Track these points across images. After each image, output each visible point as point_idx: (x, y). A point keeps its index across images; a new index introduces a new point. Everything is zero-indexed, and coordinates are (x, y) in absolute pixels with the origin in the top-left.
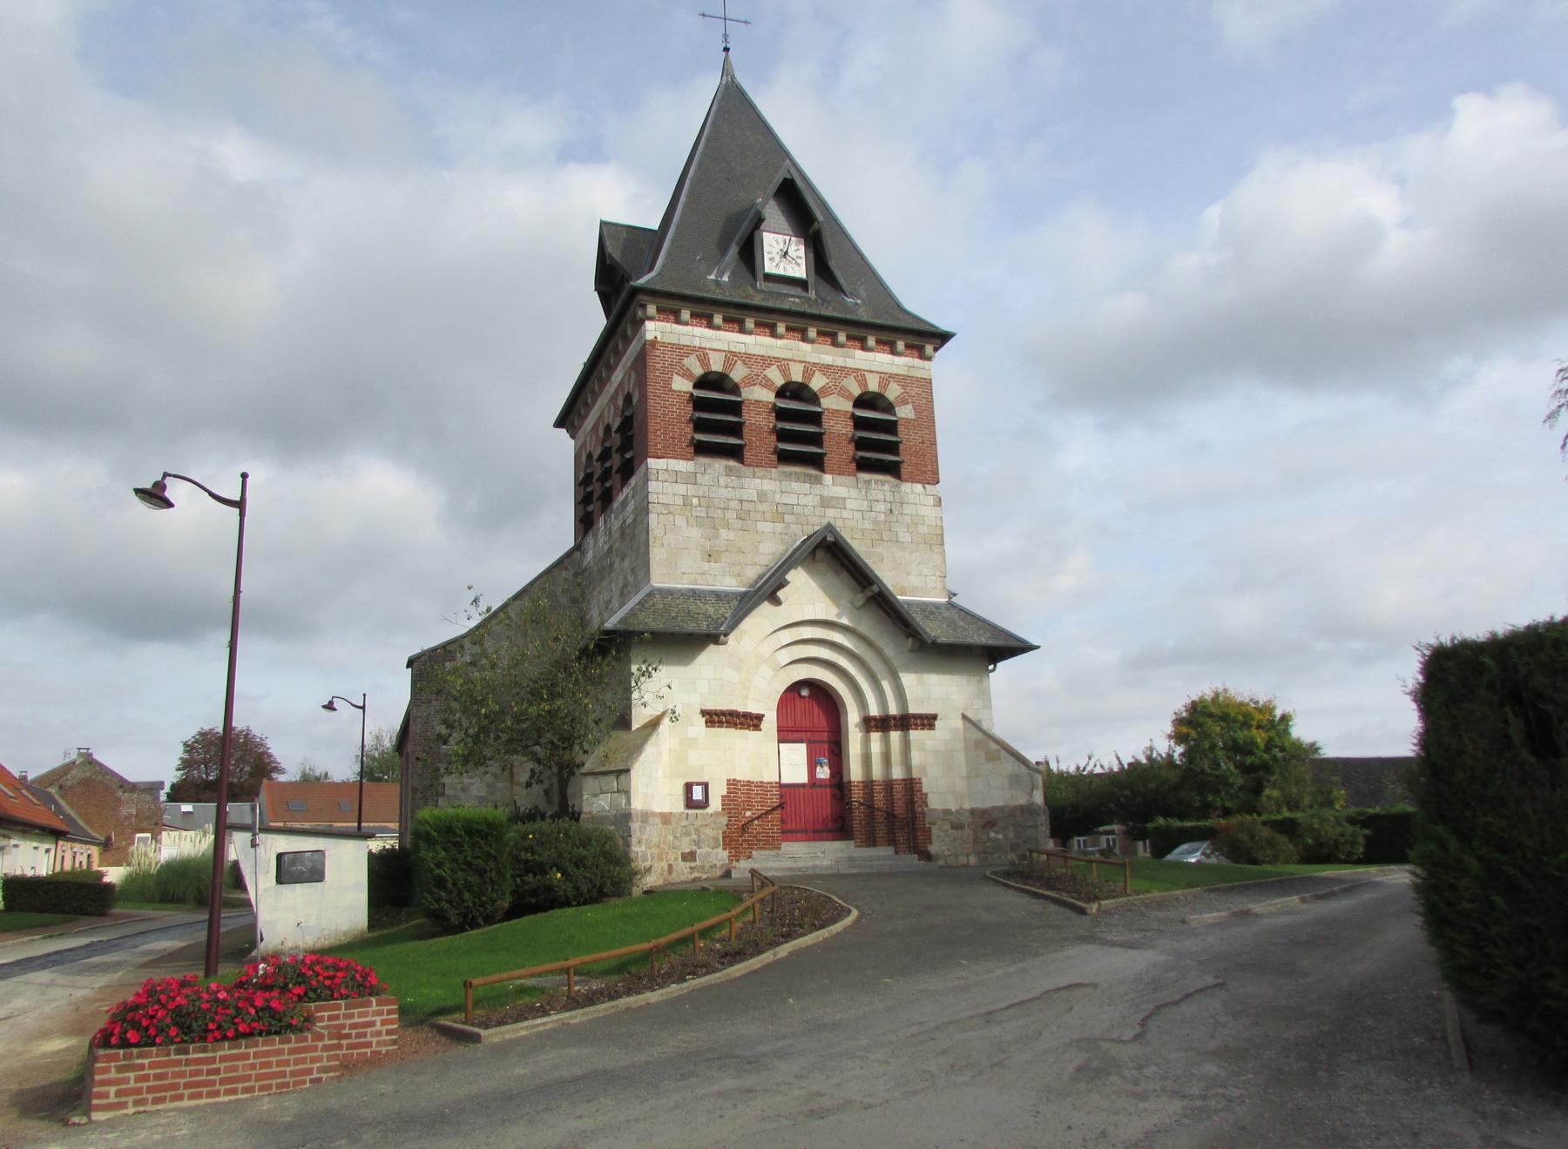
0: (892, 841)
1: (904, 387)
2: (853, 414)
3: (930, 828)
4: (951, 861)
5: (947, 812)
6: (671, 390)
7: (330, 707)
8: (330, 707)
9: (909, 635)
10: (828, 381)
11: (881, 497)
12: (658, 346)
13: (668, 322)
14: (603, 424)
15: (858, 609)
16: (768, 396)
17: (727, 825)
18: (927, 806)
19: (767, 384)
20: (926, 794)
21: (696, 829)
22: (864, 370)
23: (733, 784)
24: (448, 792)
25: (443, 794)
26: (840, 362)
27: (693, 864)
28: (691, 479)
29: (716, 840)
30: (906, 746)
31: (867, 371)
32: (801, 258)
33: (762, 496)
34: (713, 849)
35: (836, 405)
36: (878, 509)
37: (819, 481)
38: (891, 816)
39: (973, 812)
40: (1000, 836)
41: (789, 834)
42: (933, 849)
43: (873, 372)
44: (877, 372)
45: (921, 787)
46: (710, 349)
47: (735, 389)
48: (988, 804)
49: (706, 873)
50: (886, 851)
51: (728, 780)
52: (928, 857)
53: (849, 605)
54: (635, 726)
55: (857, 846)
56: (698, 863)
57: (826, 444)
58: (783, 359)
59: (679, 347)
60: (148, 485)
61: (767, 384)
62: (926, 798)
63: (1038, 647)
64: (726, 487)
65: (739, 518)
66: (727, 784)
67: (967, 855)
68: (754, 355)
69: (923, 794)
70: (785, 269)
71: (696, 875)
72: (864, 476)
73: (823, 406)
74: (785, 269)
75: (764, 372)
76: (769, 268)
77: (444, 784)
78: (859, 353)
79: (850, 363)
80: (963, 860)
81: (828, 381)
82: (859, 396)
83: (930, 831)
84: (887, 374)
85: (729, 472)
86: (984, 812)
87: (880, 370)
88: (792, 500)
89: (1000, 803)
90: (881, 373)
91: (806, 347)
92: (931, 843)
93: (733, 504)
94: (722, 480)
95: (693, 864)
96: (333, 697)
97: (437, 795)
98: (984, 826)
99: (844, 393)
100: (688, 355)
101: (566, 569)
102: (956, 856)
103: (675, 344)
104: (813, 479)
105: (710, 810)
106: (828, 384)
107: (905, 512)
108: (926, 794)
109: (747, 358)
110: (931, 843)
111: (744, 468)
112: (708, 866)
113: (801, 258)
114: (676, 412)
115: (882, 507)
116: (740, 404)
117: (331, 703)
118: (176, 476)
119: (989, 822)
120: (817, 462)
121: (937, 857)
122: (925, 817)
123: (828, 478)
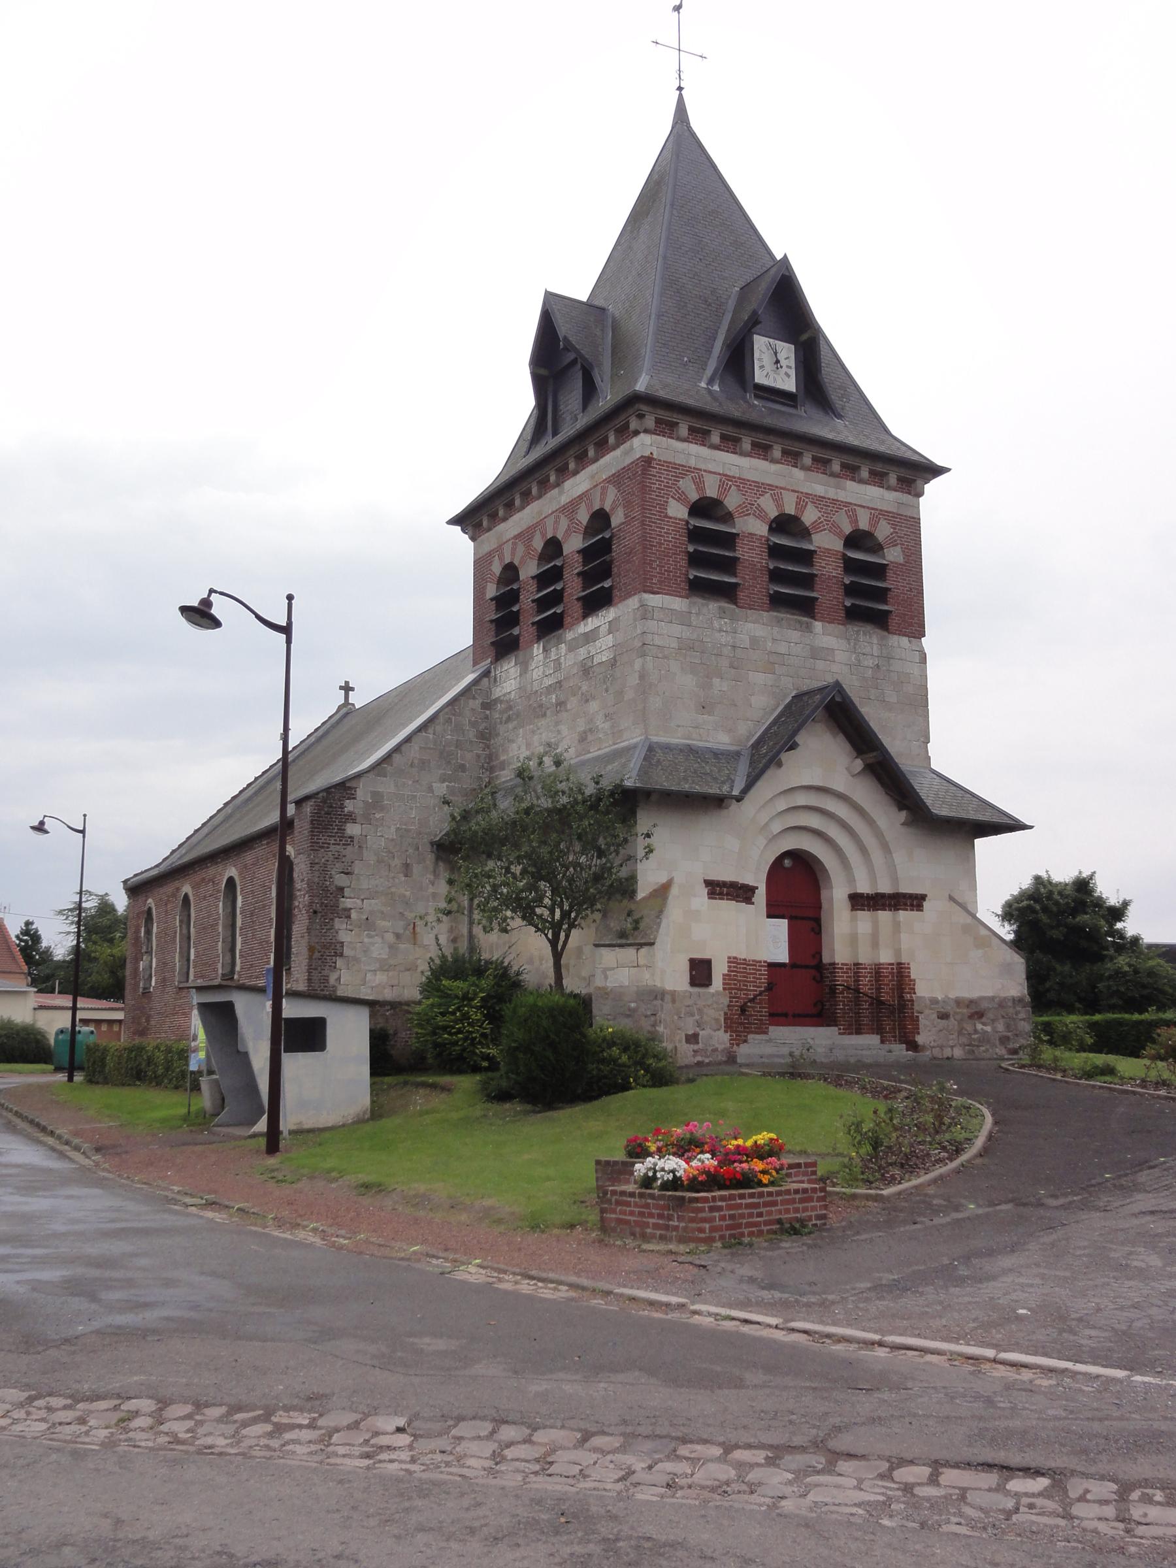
0: (879, 1030)
1: (894, 526)
2: (844, 555)
3: (918, 1017)
4: (937, 1052)
5: (934, 1001)
6: (666, 517)
7: (40, 828)
8: (40, 828)
9: (901, 807)
10: (820, 515)
11: (867, 650)
12: (654, 464)
13: (664, 436)
14: (543, 535)
15: (853, 776)
16: (761, 529)
17: (728, 1006)
18: (915, 993)
19: (760, 514)
20: (914, 980)
21: (699, 1010)
22: (855, 505)
23: (733, 961)
24: (347, 952)
25: (341, 955)
26: (831, 493)
27: (696, 1047)
28: (684, 619)
29: (717, 1020)
30: (897, 926)
31: (859, 506)
32: (790, 367)
33: (754, 641)
34: (715, 1031)
35: (827, 542)
36: (866, 663)
37: (809, 629)
38: (878, 1003)
39: (958, 1002)
40: (988, 1029)
41: (780, 1017)
42: (920, 1039)
43: (864, 507)
44: (868, 508)
45: (909, 972)
46: (705, 471)
47: (728, 517)
48: (974, 994)
49: (708, 1057)
50: (874, 1039)
51: (729, 958)
52: (913, 1046)
53: (845, 772)
54: (641, 895)
55: (840, 1034)
56: (701, 1046)
57: (817, 587)
58: (777, 487)
59: (676, 466)
60: (195, 603)
61: (760, 514)
62: (914, 985)
63: (1031, 827)
64: (720, 630)
65: (732, 666)
66: (729, 962)
67: (952, 1047)
68: (748, 481)
69: (911, 980)
70: (775, 380)
71: (699, 1058)
72: (853, 629)
73: (887, 558)
74: (775, 380)
75: (758, 501)
76: (760, 378)
77: (342, 943)
78: (850, 484)
79: (842, 496)
80: (947, 1052)
81: (820, 515)
82: (776, 518)
83: (918, 1021)
84: (877, 509)
85: (722, 613)
86: (971, 1002)
87: (871, 505)
88: (782, 648)
89: (990, 994)
90: (873, 509)
91: (798, 474)
92: (919, 1033)
93: (727, 651)
94: (716, 625)
95: (696, 1047)
96: (45, 816)
97: (336, 955)
98: (971, 1017)
99: (835, 529)
100: (683, 476)
101: (474, 698)
102: (941, 1047)
103: (670, 463)
104: (804, 626)
105: (712, 989)
106: (819, 518)
107: (891, 668)
108: (914, 980)
109: (742, 483)
110: (919, 1033)
111: (737, 610)
112: (710, 1049)
113: (790, 367)
114: (671, 541)
115: (869, 662)
116: (734, 536)
117: (42, 823)
118: (222, 593)
119: (976, 1013)
120: (727, 593)
121: (924, 1048)
122: (913, 1005)
123: (818, 626)
